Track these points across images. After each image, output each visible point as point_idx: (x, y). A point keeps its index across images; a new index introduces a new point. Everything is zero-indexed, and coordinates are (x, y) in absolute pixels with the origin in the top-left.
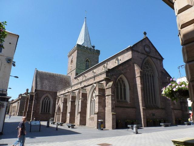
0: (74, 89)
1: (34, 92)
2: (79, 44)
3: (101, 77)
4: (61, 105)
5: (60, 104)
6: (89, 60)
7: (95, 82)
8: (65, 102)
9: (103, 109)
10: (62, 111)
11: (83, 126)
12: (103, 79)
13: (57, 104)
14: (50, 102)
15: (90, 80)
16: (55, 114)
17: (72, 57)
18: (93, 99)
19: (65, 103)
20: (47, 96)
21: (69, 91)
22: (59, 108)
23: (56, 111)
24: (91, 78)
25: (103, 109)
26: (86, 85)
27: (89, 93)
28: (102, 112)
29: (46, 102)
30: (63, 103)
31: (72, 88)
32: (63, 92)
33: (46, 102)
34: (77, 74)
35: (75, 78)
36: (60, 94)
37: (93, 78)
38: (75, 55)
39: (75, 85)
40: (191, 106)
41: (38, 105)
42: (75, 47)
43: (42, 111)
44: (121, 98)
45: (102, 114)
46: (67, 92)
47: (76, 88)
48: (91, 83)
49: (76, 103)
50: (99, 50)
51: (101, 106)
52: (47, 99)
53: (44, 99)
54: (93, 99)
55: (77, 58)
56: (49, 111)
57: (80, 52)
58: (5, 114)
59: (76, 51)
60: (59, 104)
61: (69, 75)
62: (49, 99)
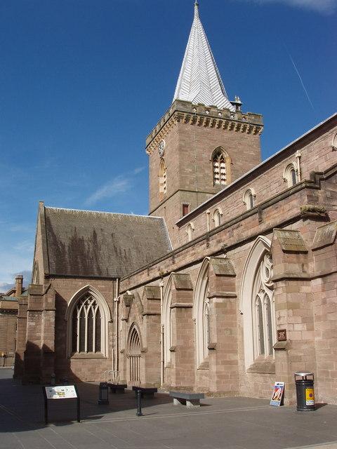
0: (183, 263)
2: (181, 98)
3: (287, 207)
7: (263, 227)
9: (308, 330)
12: (296, 212)
15: (243, 222)
24: (245, 216)
25: (308, 330)
28: (307, 342)
31: (176, 260)
35: (180, 224)
36: (133, 285)
39: (185, 247)
40: (73, 387)
44: (90, 349)
45: (304, 347)
46: (157, 274)
47: (189, 259)
48: (249, 233)
51: (299, 319)
56: (98, 349)
58: (177, 307)
62: (94, 304)
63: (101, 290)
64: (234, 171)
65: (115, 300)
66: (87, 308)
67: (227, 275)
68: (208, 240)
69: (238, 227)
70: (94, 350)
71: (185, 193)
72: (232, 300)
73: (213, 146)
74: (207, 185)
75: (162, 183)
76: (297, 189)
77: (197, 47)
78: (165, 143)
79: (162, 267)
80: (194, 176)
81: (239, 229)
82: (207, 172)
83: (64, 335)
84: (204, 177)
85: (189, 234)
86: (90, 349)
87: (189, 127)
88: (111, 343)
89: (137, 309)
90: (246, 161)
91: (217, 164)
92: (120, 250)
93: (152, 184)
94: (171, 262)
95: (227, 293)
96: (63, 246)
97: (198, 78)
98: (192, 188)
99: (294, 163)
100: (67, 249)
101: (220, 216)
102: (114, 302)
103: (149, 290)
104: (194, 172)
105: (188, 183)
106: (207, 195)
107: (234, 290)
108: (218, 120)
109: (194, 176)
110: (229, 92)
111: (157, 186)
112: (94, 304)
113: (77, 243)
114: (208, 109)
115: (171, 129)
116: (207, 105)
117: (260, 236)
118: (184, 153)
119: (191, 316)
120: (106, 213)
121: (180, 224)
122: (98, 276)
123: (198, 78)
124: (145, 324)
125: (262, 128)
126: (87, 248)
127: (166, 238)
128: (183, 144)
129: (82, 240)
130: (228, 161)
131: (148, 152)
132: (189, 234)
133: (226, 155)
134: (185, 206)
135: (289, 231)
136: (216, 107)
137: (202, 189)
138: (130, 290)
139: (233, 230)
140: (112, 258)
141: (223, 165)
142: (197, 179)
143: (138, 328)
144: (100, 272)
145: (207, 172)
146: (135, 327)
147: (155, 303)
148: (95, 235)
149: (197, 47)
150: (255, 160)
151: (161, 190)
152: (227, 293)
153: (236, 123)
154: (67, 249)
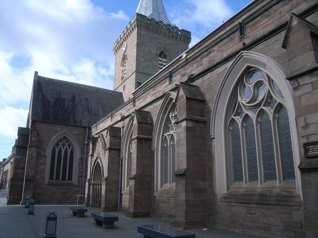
1: (30, 127)
4: (102, 157)
5: (101, 156)
6: (167, 54)
8: (115, 150)
10: (106, 175)
11: (37, 71)
13: (92, 155)
14: (72, 153)
16: (87, 184)
17: (124, 49)
18: (239, 120)
19: (113, 151)
20: (65, 138)
21: (126, 114)
22: (97, 168)
23: (88, 177)
26: (196, 72)
27: (219, 94)
29: (63, 154)
30: (110, 149)
31: (137, 103)
32: (107, 123)
33: (63, 154)
34: (138, 84)
37: (238, 33)
38: (133, 38)
41: (41, 161)
42: (132, 21)
43: (51, 177)
46: (119, 118)
49: (125, 154)
50: (188, 30)
52: (64, 145)
53: (57, 144)
54: (239, 120)
55: (138, 45)
56: (70, 178)
57: (144, 33)
59: (135, 31)
60: (95, 155)
61: (120, 90)
62: (69, 146)
66: (63, 148)
69: (210, 53)
70: (67, 179)
72: (202, 125)
79: (123, 112)
81: (211, 55)
83: (43, 167)
86: (64, 178)
88: (80, 174)
89: (101, 146)
92: (91, 109)
94: (132, 106)
95: (197, 117)
96: (49, 102)
100: (51, 104)
105: (141, 67)
113: (59, 101)
122: (73, 124)
124: (107, 157)
126: (67, 105)
129: (64, 100)
139: (202, 58)
140: (85, 113)
143: (101, 160)
144: (75, 122)
146: (99, 160)
148: (74, 98)
152: (197, 117)
154: (51, 104)
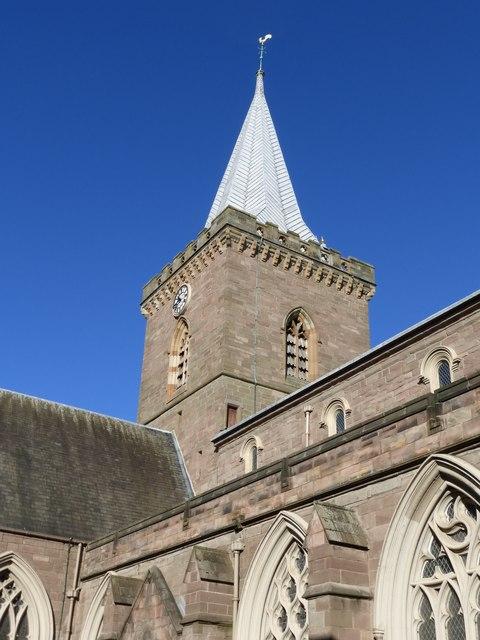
35: (220, 442)
46: (222, 522)
62: (17, 600)
63: (38, 567)
64: (323, 356)
65: (69, 594)
67: (352, 545)
68: (187, 516)
71: (234, 382)
73: (289, 304)
74: (275, 374)
75: (170, 362)
76: (259, 475)
77: (258, 127)
78: (190, 290)
79: (236, 503)
80: (252, 352)
82: (274, 349)
84: (268, 359)
85: (243, 458)
87: (246, 260)
90: (344, 342)
91: (290, 338)
93: (150, 367)
97: (257, 175)
98: (247, 375)
99: (257, 438)
101: (256, 451)
102: (65, 597)
103: (206, 558)
104: (251, 345)
105: (239, 363)
106: (274, 393)
107: (366, 581)
108: (300, 258)
109: (252, 352)
110: (308, 218)
111: (164, 371)
112: (17, 600)
114: (283, 237)
115: (208, 261)
116: (283, 229)
117: (284, 512)
118: (237, 305)
119: (366, 624)
120: (62, 406)
121: (220, 442)
123: (257, 175)
125: (374, 289)
127: (179, 472)
128: (235, 288)
130: (313, 336)
131: (145, 312)
132: (243, 458)
133: (308, 325)
134: (232, 408)
135: (334, 508)
136: (298, 235)
137: (265, 380)
138: (113, 569)
141: (305, 344)
142: (256, 359)
145: (274, 349)
147: (220, 592)
149: (258, 127)
150: (358, 342)
151: (172, 379)
153: (331, 271)
